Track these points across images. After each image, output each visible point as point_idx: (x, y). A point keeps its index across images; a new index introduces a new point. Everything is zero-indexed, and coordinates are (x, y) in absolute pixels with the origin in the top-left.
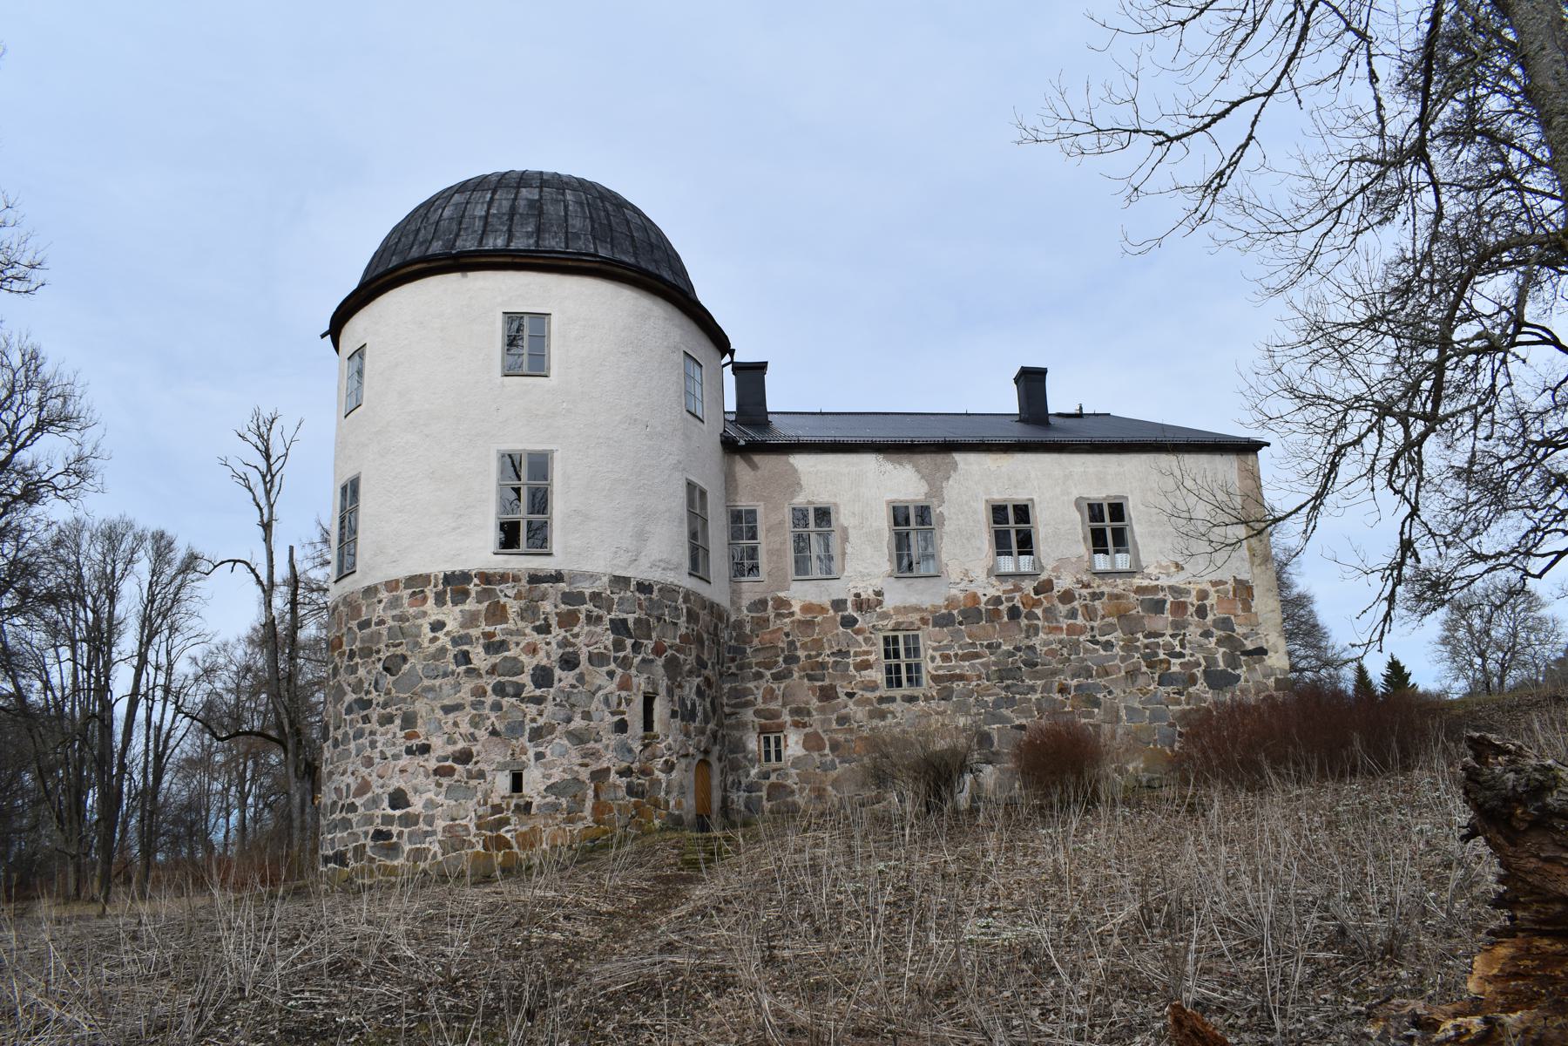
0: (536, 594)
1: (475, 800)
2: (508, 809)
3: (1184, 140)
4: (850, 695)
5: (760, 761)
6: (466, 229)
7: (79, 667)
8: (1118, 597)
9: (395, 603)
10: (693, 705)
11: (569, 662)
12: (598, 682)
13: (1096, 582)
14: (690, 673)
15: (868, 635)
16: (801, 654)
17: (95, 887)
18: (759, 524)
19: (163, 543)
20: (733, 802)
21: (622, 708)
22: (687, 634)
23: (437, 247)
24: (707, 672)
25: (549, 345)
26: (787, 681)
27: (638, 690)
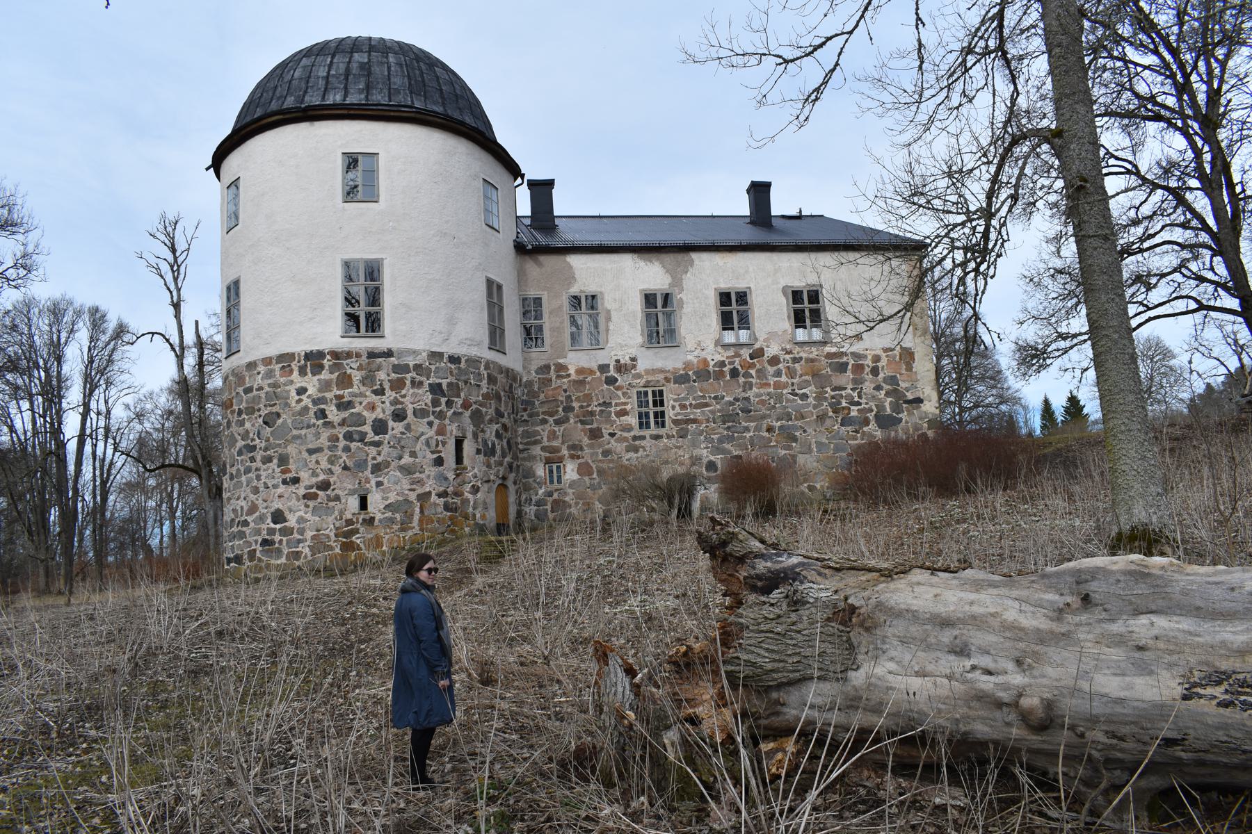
0: (374, 366)
2: (358, 522)
3: (798, 62)
4: (612, 435)
6: (312, 87)
7: (37, 415)
8: (812, 360)
9: (269, 374)
10: (493, 444)
11: (399, 416)
12: (421, 430)
13: (797, 349)
14: (491, 421)
15: (625, 390)
16: (576, 405)
17: (60, 584)
18: (543, 308)
19: (98, 315)
20: (526, 514)
23: (290, 102)
24: (504, 420)
25: (378, 178)
26: (566, 425)
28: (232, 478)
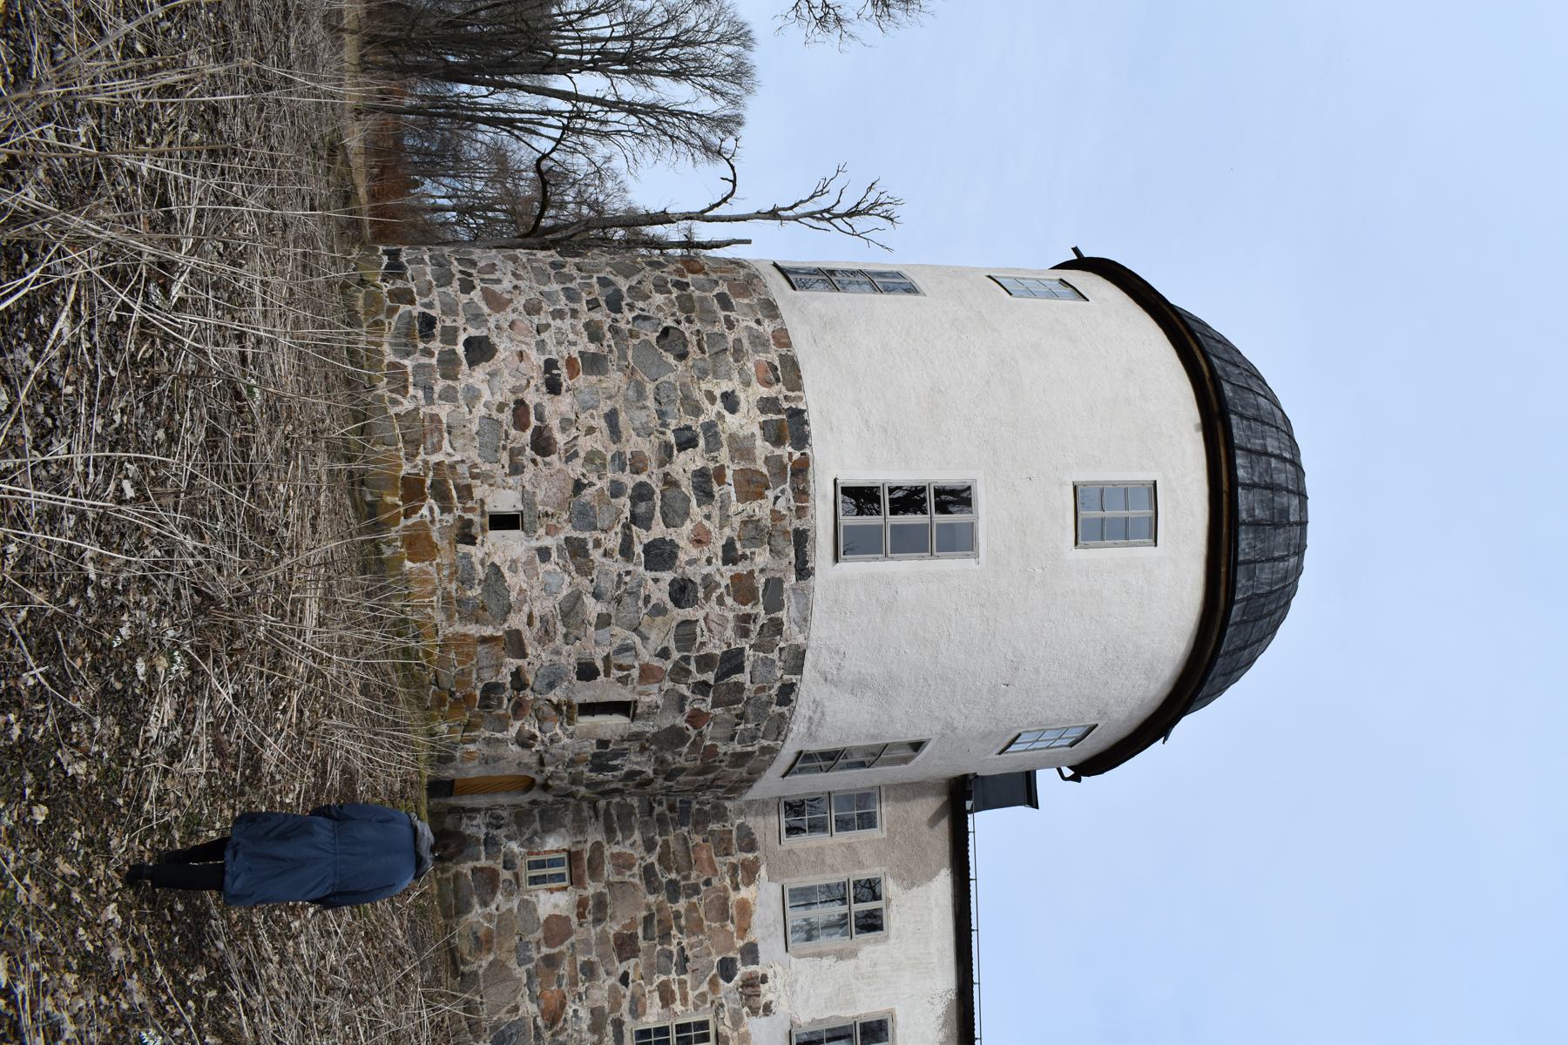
0: (780, 542)
1: (478, 461)
2: (465, 510)
4: (624, 979)
5: (530, 853)
9: (759, 342)
10: (615, 768)
11: (682, 592)
12: (653, 635)
14: (661, 761)
15: (710, 997)
16: (682, 905)
18: (857, 832)
21: (614, 671)
22: (717, 754)
25: (1116, 545)
26: (642, 887)
27: (641, 694)
28: (554, 265)
